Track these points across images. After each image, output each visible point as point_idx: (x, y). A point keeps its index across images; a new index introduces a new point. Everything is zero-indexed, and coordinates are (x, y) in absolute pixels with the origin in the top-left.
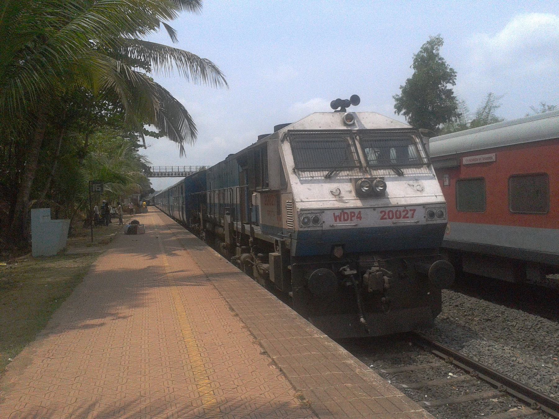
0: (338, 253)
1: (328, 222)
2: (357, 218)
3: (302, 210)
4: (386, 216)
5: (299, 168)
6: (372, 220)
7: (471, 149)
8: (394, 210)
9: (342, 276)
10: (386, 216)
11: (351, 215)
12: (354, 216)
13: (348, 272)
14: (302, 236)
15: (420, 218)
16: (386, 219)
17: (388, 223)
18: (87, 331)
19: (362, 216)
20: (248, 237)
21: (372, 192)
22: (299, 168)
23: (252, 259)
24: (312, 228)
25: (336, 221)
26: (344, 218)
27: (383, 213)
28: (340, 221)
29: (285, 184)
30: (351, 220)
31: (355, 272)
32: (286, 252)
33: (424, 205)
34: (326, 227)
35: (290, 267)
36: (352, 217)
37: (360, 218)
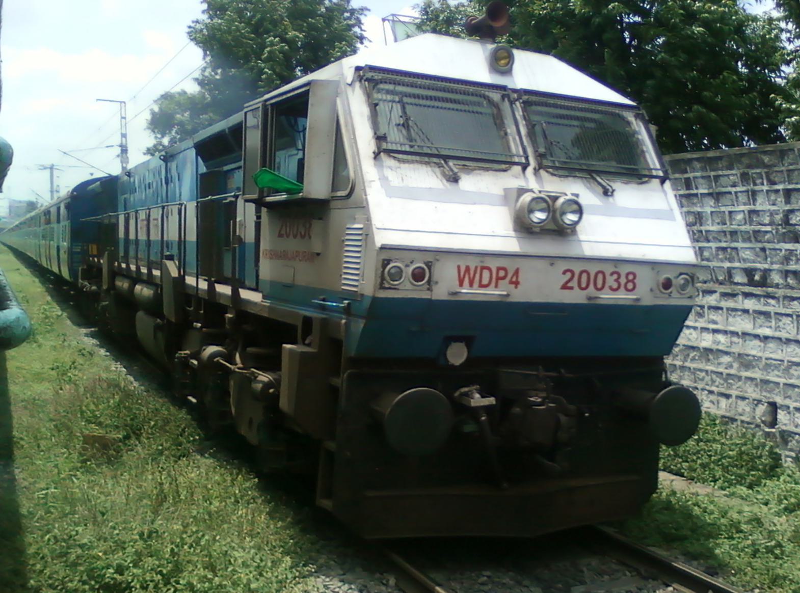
0: (457, 355)
1: (446, 285)
2: (511, 282)
3: (383, 248)
4: (574, 283)
5: (383, 149)
6: (541, 287)
7: (735, 315)
8: (593, 269)
9: (463, 410)
10: (574, 283)
11: (498, 273)
12: (504, 278)
13: (477, 400)
14: (381, 312)
15: (645, 293)
16: (571, 288)
17: (576, 297)
18: (12, 245)
19: (520, 279)
20: (224, 309)
21: (548, 225)
22: (383, 149)
23: (140, 487)
24: (407, 290)
25: (461, 284)
26: (480, 281)
27: (569, 275)
28: (471, 284)
29: (345, 188)
30: (496, 286)
31: (491, 401)
32: (333, 345)
33: (654, 265)
34: (440, 293)
35: (336, 381)
36: (499, 278)
37: (516, 284)
